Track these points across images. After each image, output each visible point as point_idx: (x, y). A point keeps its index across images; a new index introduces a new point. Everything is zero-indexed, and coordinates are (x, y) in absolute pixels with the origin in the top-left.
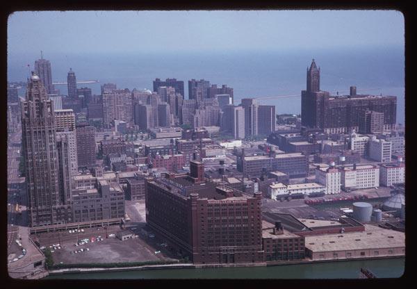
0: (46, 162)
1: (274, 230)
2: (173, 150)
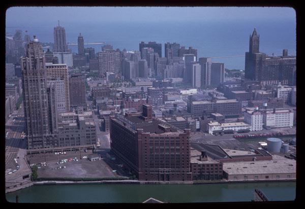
0: (39, 102)
1: (200, 157)
2: (142, 95)
